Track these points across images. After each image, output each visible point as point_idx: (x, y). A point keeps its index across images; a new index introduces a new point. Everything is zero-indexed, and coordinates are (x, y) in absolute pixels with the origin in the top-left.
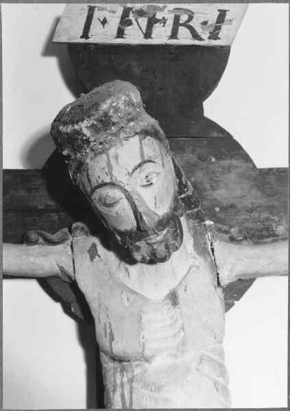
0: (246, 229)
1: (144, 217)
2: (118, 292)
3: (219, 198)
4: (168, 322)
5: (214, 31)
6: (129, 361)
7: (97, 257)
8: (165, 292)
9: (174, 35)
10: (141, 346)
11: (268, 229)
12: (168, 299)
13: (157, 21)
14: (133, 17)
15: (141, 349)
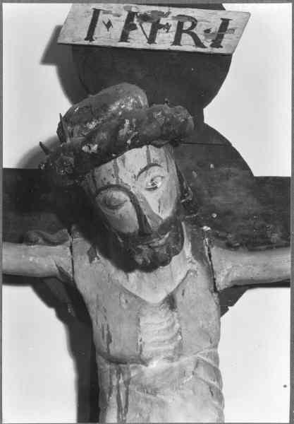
0: (242, 235)
1: (149, 220)
2: (117, 294)
3: (216, 204)
4: (165, 325)
5: (217, 39)
6: (126, 363)
7: (96, 259)
8: (162, 296)
9: (177, 41)
10: (139, 348)
11: (263, 236)
12: (166, 302)
13: (162, 27)
14: (138, 21)
15: (139, 352)
